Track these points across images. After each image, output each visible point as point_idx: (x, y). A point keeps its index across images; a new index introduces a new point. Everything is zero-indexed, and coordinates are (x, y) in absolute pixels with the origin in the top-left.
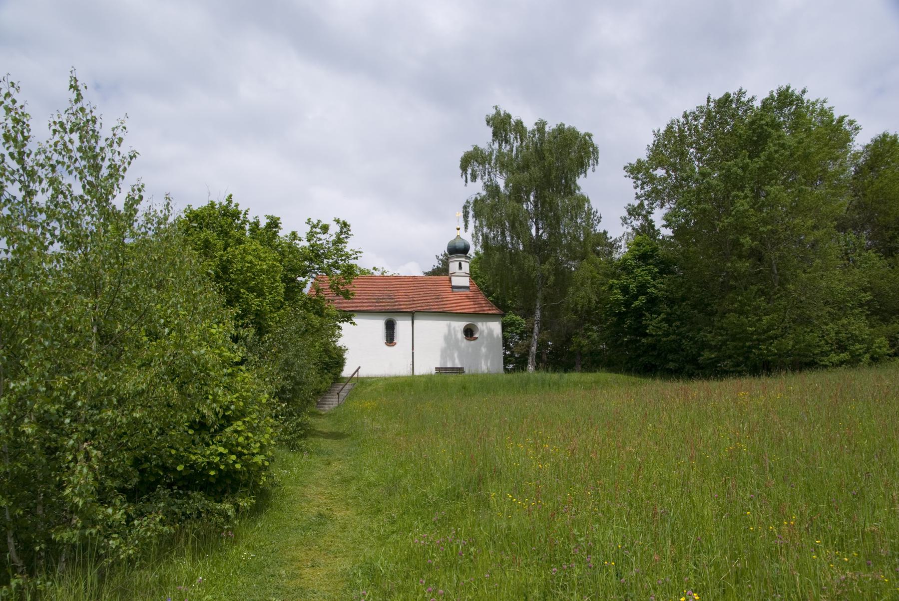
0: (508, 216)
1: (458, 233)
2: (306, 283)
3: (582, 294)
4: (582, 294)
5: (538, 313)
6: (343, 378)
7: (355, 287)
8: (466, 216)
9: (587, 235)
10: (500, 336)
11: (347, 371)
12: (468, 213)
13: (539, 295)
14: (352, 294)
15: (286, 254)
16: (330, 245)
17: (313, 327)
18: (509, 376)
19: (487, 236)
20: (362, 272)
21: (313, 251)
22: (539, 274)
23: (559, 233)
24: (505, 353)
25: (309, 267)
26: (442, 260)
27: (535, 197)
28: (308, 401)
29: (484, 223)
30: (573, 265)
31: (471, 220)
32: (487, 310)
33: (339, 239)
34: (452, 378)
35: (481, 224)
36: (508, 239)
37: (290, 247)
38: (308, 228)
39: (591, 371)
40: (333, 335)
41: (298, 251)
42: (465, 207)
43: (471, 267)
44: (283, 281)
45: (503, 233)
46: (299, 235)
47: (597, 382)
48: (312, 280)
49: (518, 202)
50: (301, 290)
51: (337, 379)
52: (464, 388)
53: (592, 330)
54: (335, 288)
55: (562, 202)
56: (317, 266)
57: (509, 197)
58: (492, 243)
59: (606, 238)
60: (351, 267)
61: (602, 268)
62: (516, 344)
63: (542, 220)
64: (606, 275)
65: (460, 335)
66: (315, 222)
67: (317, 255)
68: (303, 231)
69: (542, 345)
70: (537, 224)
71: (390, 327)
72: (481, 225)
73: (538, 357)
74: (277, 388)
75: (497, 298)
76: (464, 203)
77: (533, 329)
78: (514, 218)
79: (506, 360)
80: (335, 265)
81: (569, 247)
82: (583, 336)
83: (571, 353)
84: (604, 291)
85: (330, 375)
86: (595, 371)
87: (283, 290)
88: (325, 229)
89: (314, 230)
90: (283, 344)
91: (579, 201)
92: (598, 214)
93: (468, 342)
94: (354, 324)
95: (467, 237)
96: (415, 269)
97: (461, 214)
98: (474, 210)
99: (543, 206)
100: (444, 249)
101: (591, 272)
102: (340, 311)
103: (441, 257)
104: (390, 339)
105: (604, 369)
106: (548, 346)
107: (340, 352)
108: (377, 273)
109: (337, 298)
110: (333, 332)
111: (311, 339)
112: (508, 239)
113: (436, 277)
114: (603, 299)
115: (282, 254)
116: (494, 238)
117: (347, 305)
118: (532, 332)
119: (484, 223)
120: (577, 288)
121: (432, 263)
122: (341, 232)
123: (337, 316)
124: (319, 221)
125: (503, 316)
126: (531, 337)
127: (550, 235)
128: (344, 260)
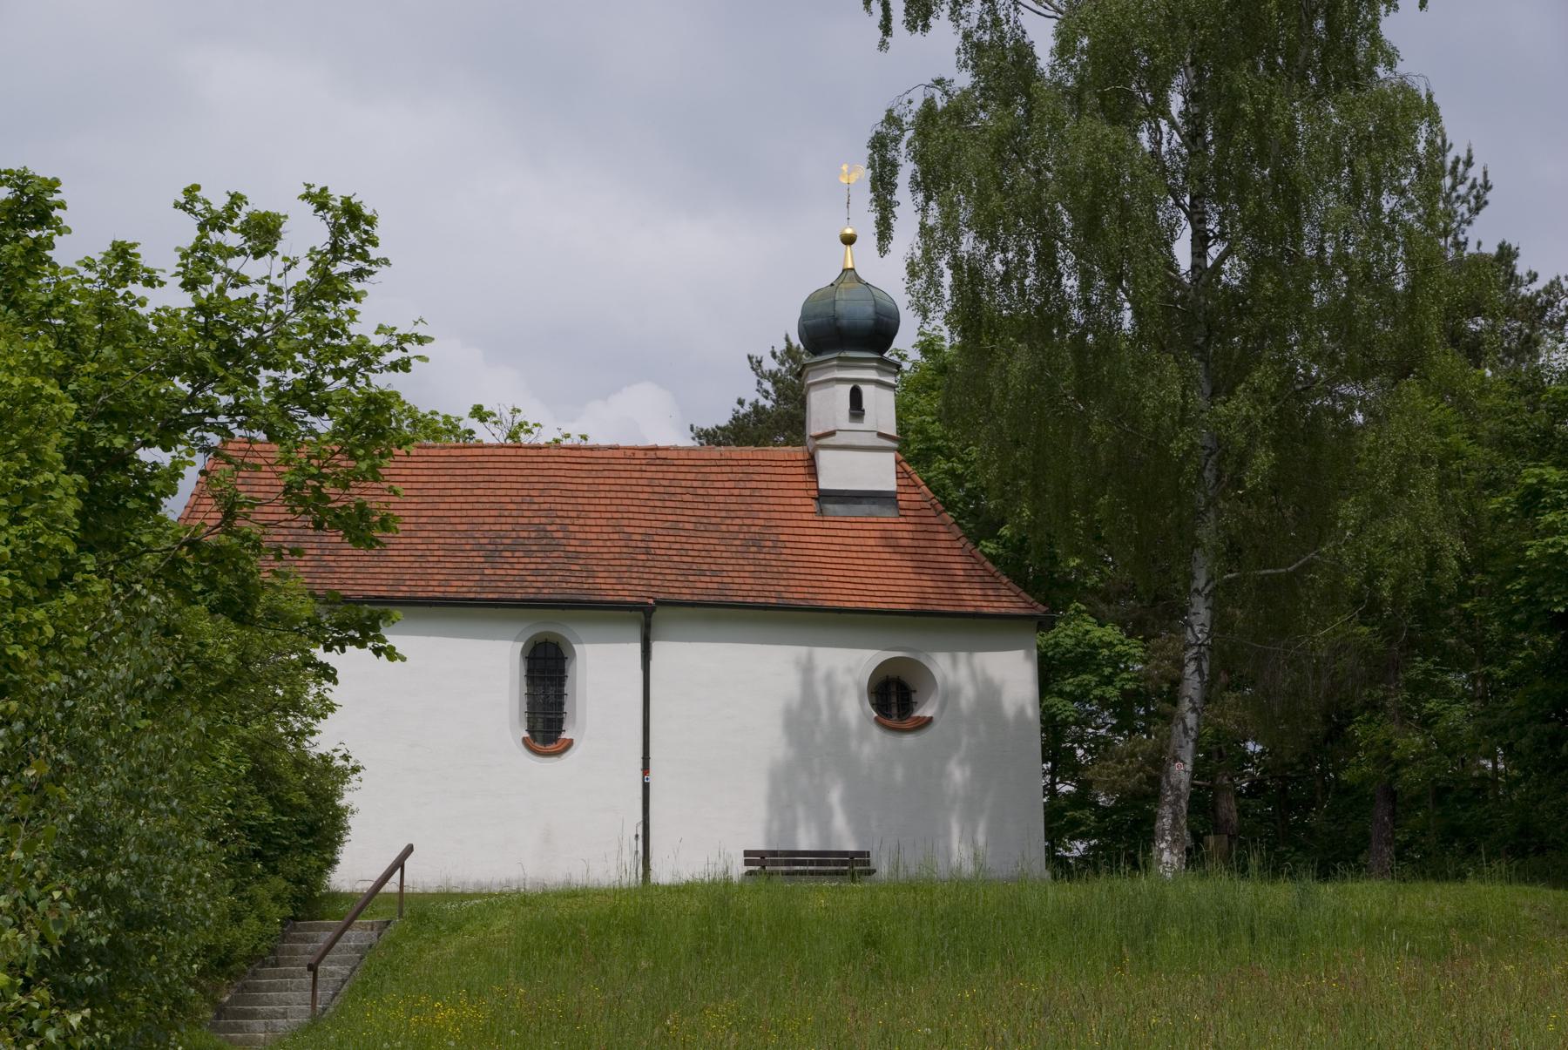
0: (1070, 182)
1: (849, 257)
2: (175, 473)
3: (1398, 527)
4: (1398, 527)
5: (1201, 614)
6: (336, 897)
7: (399, 488)
8: (883, 182)
9: (1424, 266)
10: (1032, 713)
11: (355, 867)
12: (894, 166)
13: (1207, 532)
14: (384, 524)
15: (88, 341)
16: (287, 307)
17: (206, 668)
18: (1071, 893)
19: (975, 273)
20: (426, 426)
21: (207, 333)
22: (1204, 438)
23: (1296, 258)
24: (1051, 791)
25: (191, 400)
26: (773, 377)
27: (1192, 97)
28: (178, 1003)
29: (964, 214)
30: (1356, 402)
31: (906, 200)
32: (973, 598)
33: (325, 277)
34: (819, 897)
35: (949, 215)
36: (1070, 283)
37: (103, 314)
38: (186, 230)
39: (1439, 876)
40: (294, 704)
41: (140, 330)
42: (879, 144)
43: (902, 410)
44: (73, 465)
45: (1047, 260)
46: (148, 258)
47: (1469, 925)
48: (200, 460)
49: (1113, 121)
50: (155, 505)
51: (310, 903)
52: (871, 941)
53: (1443, 691)
54: (305, 497)
55: (1315, 121)
56: (226, 400)
57: (1077, 97)
58: (1000, 303)
59: (1512, 277)
60: (379, 404)
61: (1492, 412)
62: (1100, 748)
63: (1220, 198)
64: (1507, 444)
65: (855, 708)
66: (219, 203)
67: (229, 352)
68: (164, 240)
69: (1217, 754)
70: (1197, 218)
71: (546, 673)
72: (951, 226)
73: (1202, 806)
74: (43, 942)
75: (1019, 547)
76: (871, 122)
77: (1176, 683)
78: (1098, 193)
79: (1059, 821)
80: (309, 396)
81: (1341, 317)
82: (1404, 715)
83: (1345, 790)
84: (1499, 517)
85: (278, 883)
86: (1461, 876)
87: (71, 506)
88: (264, 233)
89: (215, 236)
90: (73, 745)
91: (1389, 115)
92: (1475, 173)
93: (890, 740)
94: (391, 654)
95: (888, 274)
96: (651, 417)
97: (860, 175)
98: (919, 158)
99: (1224, 136)
100: (784, 327)
101: (1441, 431)
102: (332, 600)
103: (770, 365)
104: (546, 724)
105: (1500, 866)
106: (1247, 758)
107: (327, 778)
108: (486, 434)
109: (313, 543)
110: (298, 692)
111: (200, 723)
112: (1070, 283)
113: (748, 451)
114: (1494, 554)
115: (69, 341)
116: (1006, 278)
117: (357, 572)
118: (1174, 698)
119: (964, 214)
120: (1378, 501)
121: (732, 392)
122: (336, 249)
123: (314, 622)
124: (236, 200)
125: (1045, 624)
126: (1168, 718)
127: (1258, 264)
128: (350, 373)
